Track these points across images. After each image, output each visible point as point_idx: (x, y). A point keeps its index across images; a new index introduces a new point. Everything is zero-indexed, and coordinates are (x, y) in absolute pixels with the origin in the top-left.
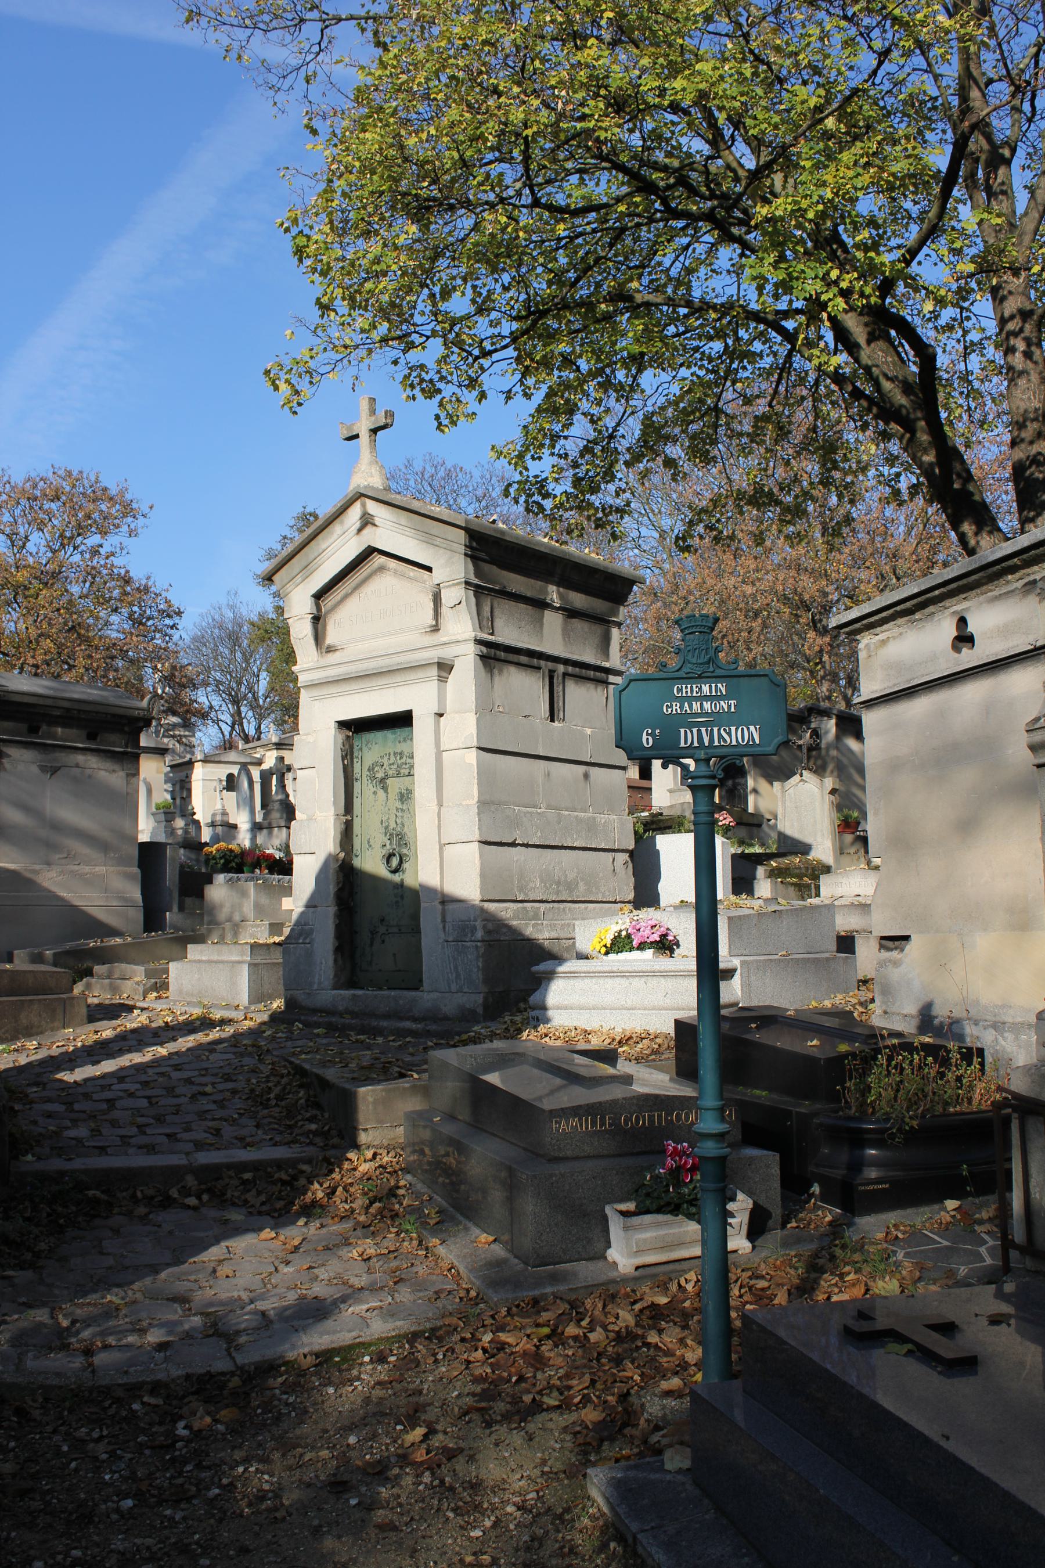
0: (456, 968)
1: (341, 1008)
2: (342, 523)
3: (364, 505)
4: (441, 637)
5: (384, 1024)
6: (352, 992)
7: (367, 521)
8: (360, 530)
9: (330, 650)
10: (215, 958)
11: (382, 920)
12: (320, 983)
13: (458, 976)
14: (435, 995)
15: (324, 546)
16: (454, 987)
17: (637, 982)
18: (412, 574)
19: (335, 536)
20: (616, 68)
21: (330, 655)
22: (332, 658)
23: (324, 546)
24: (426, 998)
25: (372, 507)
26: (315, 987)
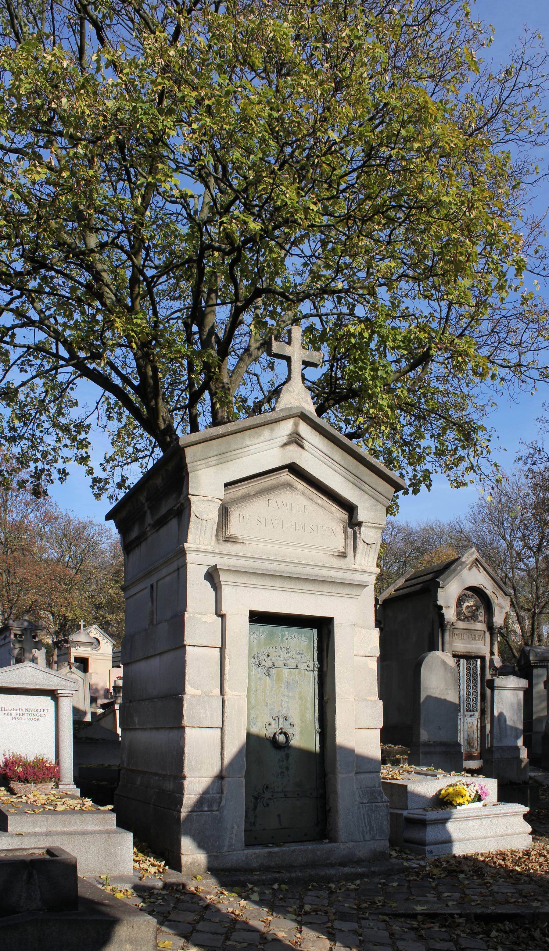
0: (370, 822)
1: (255, 865)
2: (272, 430)
3: (296, 425)
4: (348, 562)
5: (332, 872)
6: (267, 850)
7: (296, 440)
8: (285, 445)
9: (230, 539)
10: (60, 828)
11: (267, 787)
12: (230, 845)
13: (371, 829)
14: (350, 845)
15: (248, 443)
16: (367, 837)
17: (486, 821)
18: (320, 501)
19: (262, 438)
20: (505, 201)
21: (229, 544)
22: (228, 547)
23: (248, 443)
24: (342, 847)
25: (304, 429)
26: (225, 849)
